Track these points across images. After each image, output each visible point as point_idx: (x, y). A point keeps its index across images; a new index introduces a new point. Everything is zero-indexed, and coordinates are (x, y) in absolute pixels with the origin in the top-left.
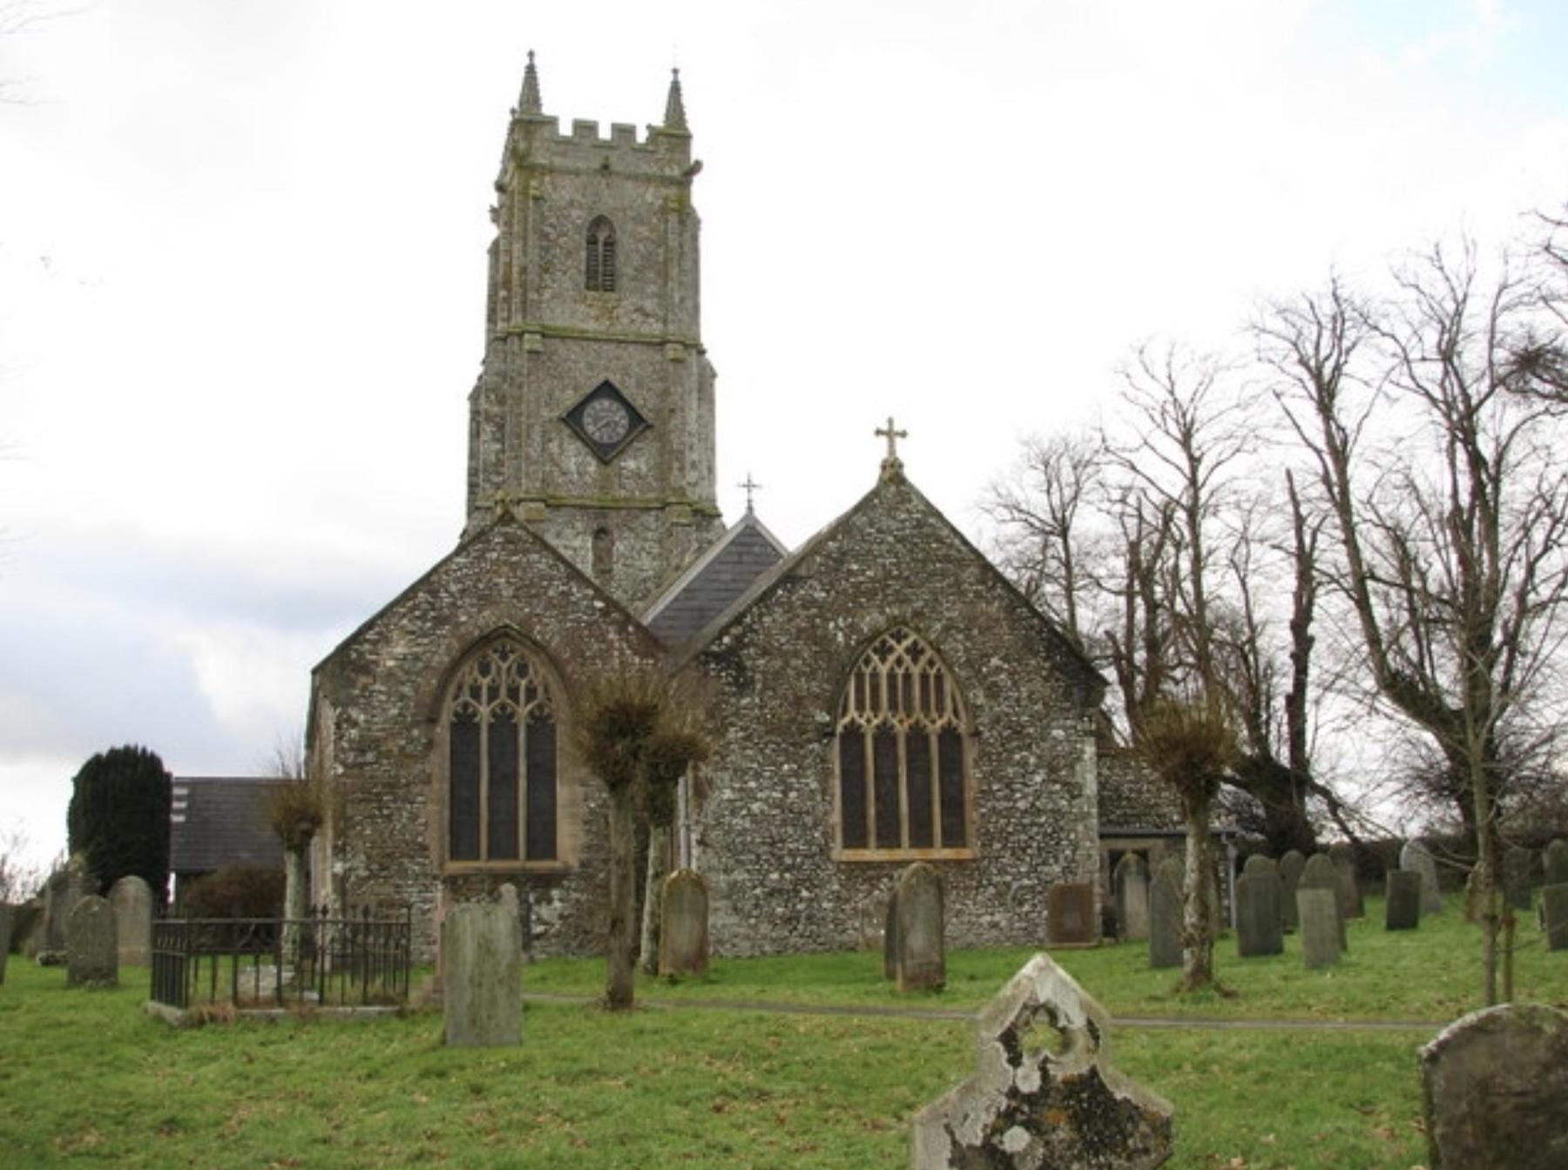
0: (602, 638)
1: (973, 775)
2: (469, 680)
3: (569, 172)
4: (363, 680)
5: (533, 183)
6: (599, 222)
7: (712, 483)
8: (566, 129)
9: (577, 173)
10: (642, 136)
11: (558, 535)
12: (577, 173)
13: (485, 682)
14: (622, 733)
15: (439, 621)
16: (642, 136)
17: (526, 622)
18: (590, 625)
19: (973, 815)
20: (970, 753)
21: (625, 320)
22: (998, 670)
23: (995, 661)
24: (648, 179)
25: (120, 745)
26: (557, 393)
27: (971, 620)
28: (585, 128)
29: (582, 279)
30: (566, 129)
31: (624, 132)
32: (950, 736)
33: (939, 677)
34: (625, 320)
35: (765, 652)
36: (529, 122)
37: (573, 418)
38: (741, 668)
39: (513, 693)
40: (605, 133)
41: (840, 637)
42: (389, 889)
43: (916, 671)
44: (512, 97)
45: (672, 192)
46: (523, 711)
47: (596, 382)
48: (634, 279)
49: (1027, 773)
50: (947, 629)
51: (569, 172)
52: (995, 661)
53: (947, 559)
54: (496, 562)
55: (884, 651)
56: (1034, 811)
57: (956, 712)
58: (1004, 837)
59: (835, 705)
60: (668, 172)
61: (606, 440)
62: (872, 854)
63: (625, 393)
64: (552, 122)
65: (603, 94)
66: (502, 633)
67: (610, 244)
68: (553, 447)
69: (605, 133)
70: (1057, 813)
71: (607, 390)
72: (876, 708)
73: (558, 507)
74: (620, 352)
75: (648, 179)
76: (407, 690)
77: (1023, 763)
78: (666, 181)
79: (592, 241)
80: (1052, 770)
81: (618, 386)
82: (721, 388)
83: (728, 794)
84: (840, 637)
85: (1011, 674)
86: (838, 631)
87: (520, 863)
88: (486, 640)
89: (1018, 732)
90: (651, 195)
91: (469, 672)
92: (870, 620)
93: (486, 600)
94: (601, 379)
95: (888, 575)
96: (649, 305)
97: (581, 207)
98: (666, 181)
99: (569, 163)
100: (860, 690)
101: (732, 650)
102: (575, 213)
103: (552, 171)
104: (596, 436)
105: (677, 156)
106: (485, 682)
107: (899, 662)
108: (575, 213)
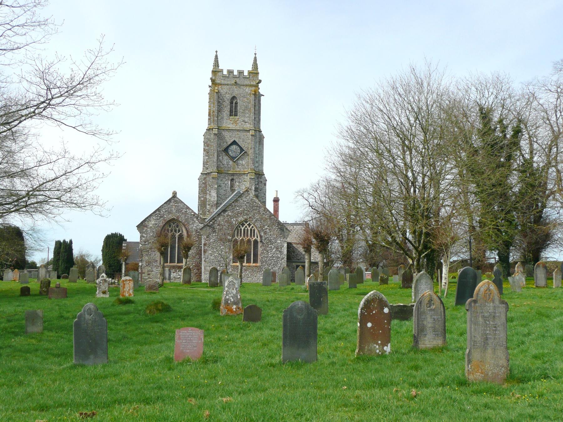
0: (193, 220)
1: (260, 249)
2: (167, 228)
3: (226, 85)
4: (145, 228)
5: (216, 88)
6: (234, 98)
7: (262, 166)
8: (225, 72)
9: (228, 85)
10: (246, 73)
11: (221, 180)
12: (228, 85)
13: (170, 229)
14: (163, 246)
15: (161, 217)
16: (246, 73)
17: (178, 217)
18: (191, 218)
19: (259, 257)
20: (260, 245)
21: (240, 124)
22: (266, 229)
23: (266, 227)
24: (247, 86)
25: (114, 232)
26: (222, 144)
27: (262, 219)
28: (230, 72)
29: (229, 113)
30: (225, 72)
31: (241, 72)
32: (256, 242)
33: (254, 230)
34: (240, 124)
35: (219, 225)
36: (216, 71)
37: (226, 150)
38: (214, 228)
39: (175, 231)
40: (236, 73)
41: (234, 222)
42: (150, 268)
43: (249, 229)
44: (211, 68)
45: (253, 88)
46: (177, 235)
47: (232, 141)
48: (243, 113)
49: (272, 249)
50: (256, 220)
51: (226, 85)
52: (266, 227)
53: (257, 206)
54: (172, 205)
55: (243, 225)
56: (272, 257)
57: (257, 237)
58: (266, 261)
59: (233, 236)
60: (252, 83)
61: (234, 156)
62: (252, 264)
63: (239, 143)
64: (222, 71)
65: (236, 62)
66: (173, 219)
67: (236, 103)
68: (221, 158)
69: (236, 73)
70: (278, 258)
71: (234, 143)
72: (241, 236)
73: (221, 173)
74: (239, 133)
75: (247, 86)
76: (154, 230)
77: (271, 247)
78: (251, 86)
79: (232, 103)
80: (277, 249)
81: (237, 141)
82: (266, 141)
83: (210, 252)
84: (234, 222)
85: (269, 229)
86: (234, 221)
87: (176, 264)
88: (170, 221)
89: (270, 241)
90: (248, 90)
91: (167, 227)
92: (241, 219)
93: (170, 213)
94: (233, 140)
95: (245, 210)
96: (246, 120)
97: (229, 94)
98: (251, 86)
99: (226, 82)
100: (238, 233)
101: (212, 225)
102: (227, 95)
103: (221, 84)
104: (232, 155)
105: (255, 78)
106: (170, 229)
107: (246, 227)
108: (227, 95)
